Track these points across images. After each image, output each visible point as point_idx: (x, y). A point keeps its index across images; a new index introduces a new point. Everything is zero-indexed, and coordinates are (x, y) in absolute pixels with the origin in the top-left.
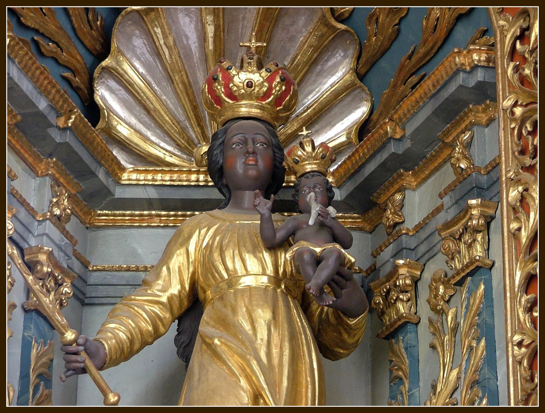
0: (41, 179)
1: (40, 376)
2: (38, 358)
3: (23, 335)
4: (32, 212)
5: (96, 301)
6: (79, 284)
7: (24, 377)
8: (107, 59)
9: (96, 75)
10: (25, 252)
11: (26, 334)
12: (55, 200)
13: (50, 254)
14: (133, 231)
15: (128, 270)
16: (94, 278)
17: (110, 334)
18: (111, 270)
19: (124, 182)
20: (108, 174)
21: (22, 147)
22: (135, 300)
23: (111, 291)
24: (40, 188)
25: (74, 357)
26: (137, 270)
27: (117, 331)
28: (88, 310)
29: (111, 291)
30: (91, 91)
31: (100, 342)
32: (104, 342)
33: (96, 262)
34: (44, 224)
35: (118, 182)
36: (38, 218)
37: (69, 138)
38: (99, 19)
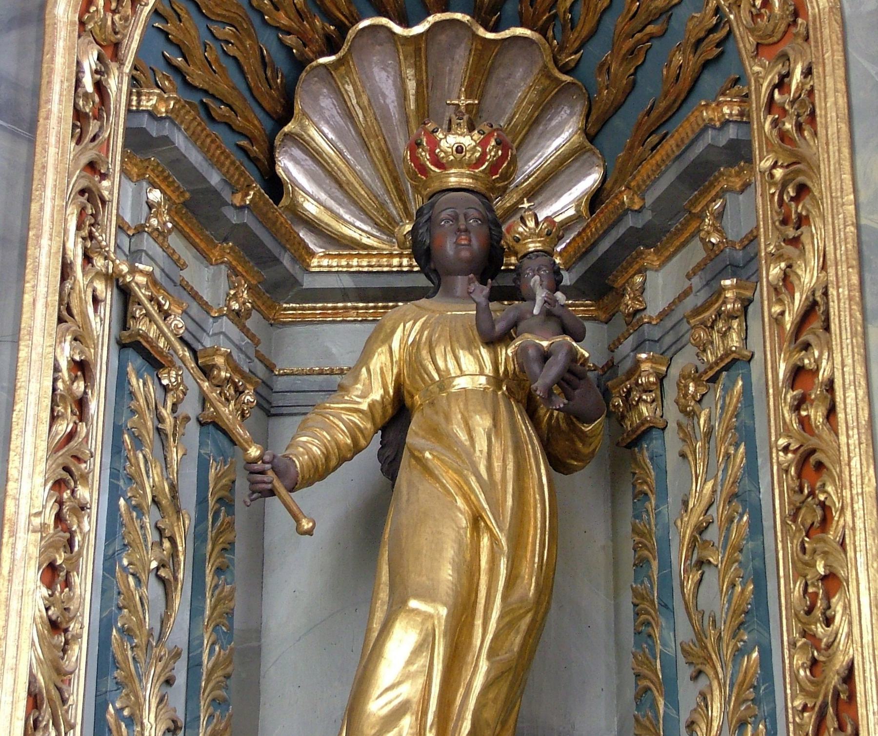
0: (216, 267)
2: (218, 479)
5: (285, 411)
7: (202, 501)
9: (277, 142)
10: (199, 354)
11: (202, 452)
12: (232, 292)
13: (228, 357)
14: (325, 326)
15: (321, 373)
16: (280, 384)
17: (301, 449)
19: (313, 270)
20: (295, 260)
21: (192, 230)
22: (330, 408)
24: (215, 278)
25: (259, 477)
26: (332, 373)
27: (310, 446)
29: (301, 398)
31: (291, 459)
33: (283, 365)
35: (306, 269)
37: (247, 218)
38: (280, 76)
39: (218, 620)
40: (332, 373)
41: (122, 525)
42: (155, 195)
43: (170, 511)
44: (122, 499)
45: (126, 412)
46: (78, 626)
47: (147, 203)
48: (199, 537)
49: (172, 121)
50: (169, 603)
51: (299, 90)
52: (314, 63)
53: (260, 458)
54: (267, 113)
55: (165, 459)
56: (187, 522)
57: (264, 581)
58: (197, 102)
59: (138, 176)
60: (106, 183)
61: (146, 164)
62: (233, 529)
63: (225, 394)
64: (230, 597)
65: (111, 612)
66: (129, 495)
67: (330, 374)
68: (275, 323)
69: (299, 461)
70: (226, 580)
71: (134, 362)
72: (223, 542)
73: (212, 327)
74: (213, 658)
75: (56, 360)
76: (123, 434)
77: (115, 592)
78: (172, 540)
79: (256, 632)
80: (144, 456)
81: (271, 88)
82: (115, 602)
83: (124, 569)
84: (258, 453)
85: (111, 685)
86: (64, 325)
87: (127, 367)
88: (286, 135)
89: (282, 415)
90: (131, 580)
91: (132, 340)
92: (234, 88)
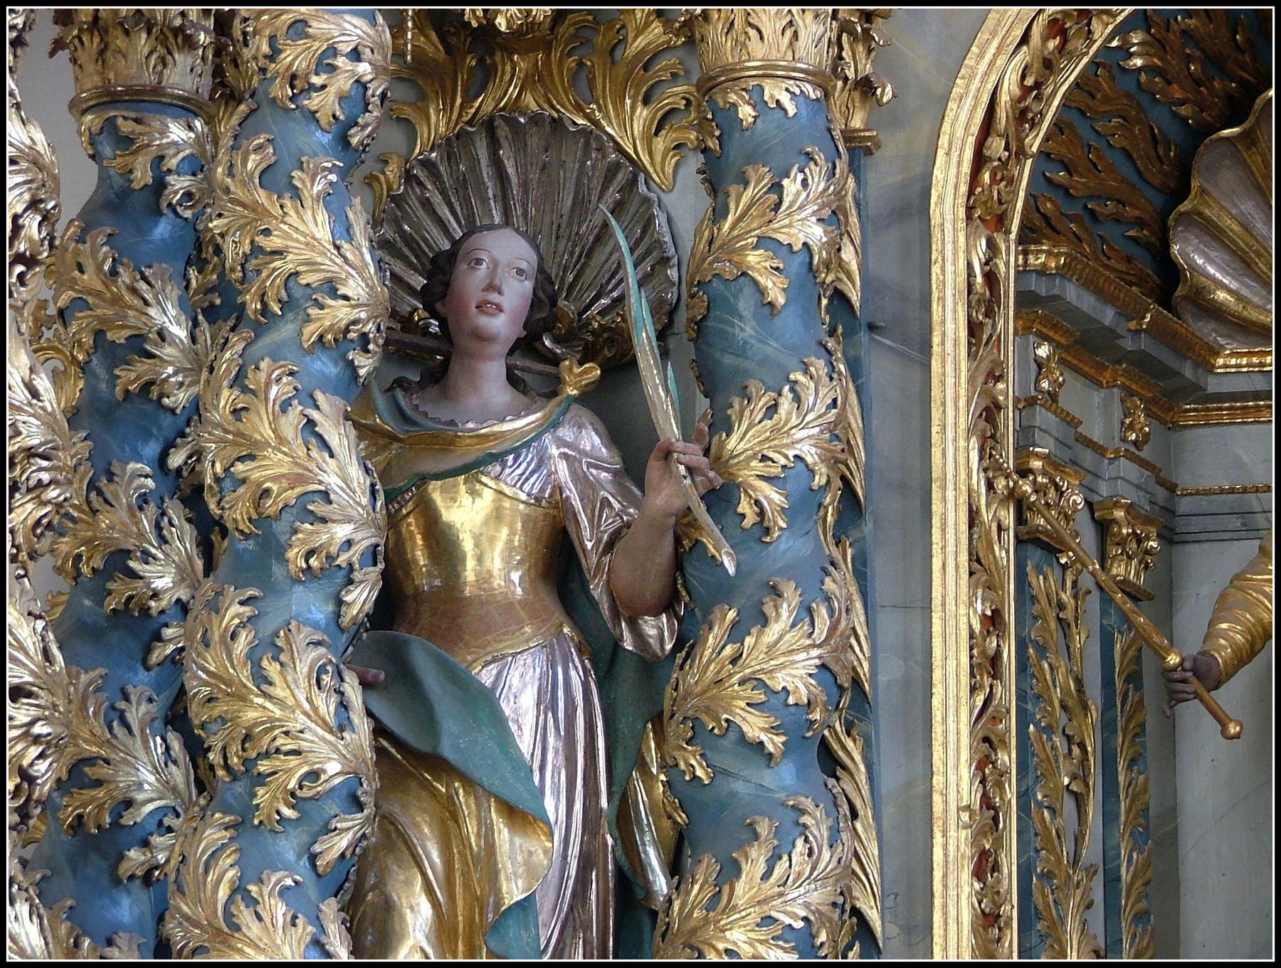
0: (1107, 391)
1: (1127, 680)
2: (1124, 653)
3: (1102, 625)
4: (1099, 450)
5: (1190, 538)
6: (1165, 532)
7: (1108, 683)
8: (1186, 202)
9: (1171, 222)
10: (1095, 507)
11: (1105, 622)
12: (1127, 421)
13: (1129, 509)
14: (1232, 428)
15: (1232, 491)
16: (1185, 505)
17: (1222, 641)
18: (1208, 492)
19: (1219, 371)
20: (1197, 365)
21: (1081, 361)
22: (1252, 580)
23: (1209, 523)
24: (1106, 404)
25: (1180, 686)
26: (1245, 491)
27: (1231, 634)
28: (1177, 550)
29: (1209, 523)
30: (1166, 246)
31: (1212, 655)
32: (1217, 655)
33: (1185, 480)
34: (1116, 462)
35: (1210, 369)
36: (1108, 456)
37: (1144, 343)
38: (1173, 148)
39: (1135, 822)
40: (1245, 491)
41: (1033, 755)
42: (1043, 351)
43: (1078, 710)
44: (1031, 726)
45: (1029, 620)
46: (1008, 907)
47: (1035, 361)
48: (1108, 727)
49: (1063, 276)
50: (1083, 817)
51: (1195, 166)
52: (1214, 136)
53: (1181, 664)
54: (1159, 190)
55: (1068, 648)
56: (1094, 715)
57: (1177, 747)
58: (1080, 211)
59: (1024, 329)
60: (1001, 386)
61: (1032, 317)
62: (1143, 707)
63: (1128, 553)
64: (1145, 790)
65: (1029, 857)
66: (1038, 717)
67: (1242, 493)
68: (1175, 427)
69: (1220, 654)
70: (1138, 770)
71: (1035, 555)
72: (1134, 727)
73: (1108, 470)
74: (1132, 869)
75: (970, 626)
76: (1028, 648)
77: (1032, 835)
78: (1082, 746)
79: (1172, 812)
80: (1050, 665)
81: (1162, 164)
82: (1033, 846)
83: (1039, 804)
84: (1178, 660)
85: (1035, 939)
86: (974, 577)
87: (1026, 566)
88: (1181, 214)
89: (1188, 542)
90: (1046, 813)
91: (1032, 536)
92: (1124, 180)
